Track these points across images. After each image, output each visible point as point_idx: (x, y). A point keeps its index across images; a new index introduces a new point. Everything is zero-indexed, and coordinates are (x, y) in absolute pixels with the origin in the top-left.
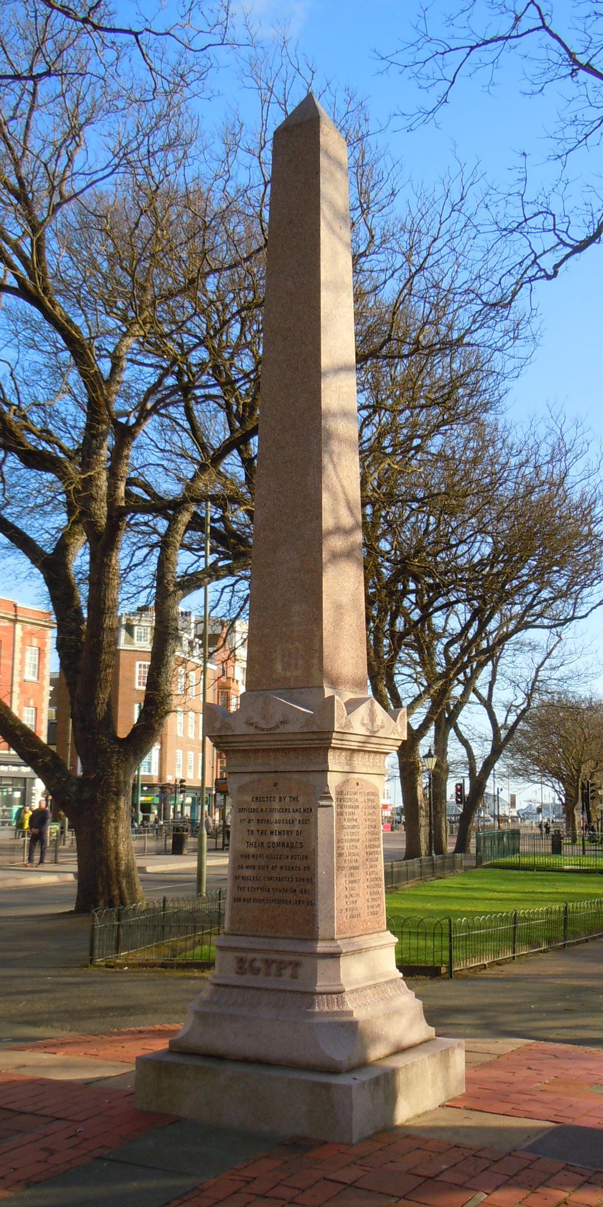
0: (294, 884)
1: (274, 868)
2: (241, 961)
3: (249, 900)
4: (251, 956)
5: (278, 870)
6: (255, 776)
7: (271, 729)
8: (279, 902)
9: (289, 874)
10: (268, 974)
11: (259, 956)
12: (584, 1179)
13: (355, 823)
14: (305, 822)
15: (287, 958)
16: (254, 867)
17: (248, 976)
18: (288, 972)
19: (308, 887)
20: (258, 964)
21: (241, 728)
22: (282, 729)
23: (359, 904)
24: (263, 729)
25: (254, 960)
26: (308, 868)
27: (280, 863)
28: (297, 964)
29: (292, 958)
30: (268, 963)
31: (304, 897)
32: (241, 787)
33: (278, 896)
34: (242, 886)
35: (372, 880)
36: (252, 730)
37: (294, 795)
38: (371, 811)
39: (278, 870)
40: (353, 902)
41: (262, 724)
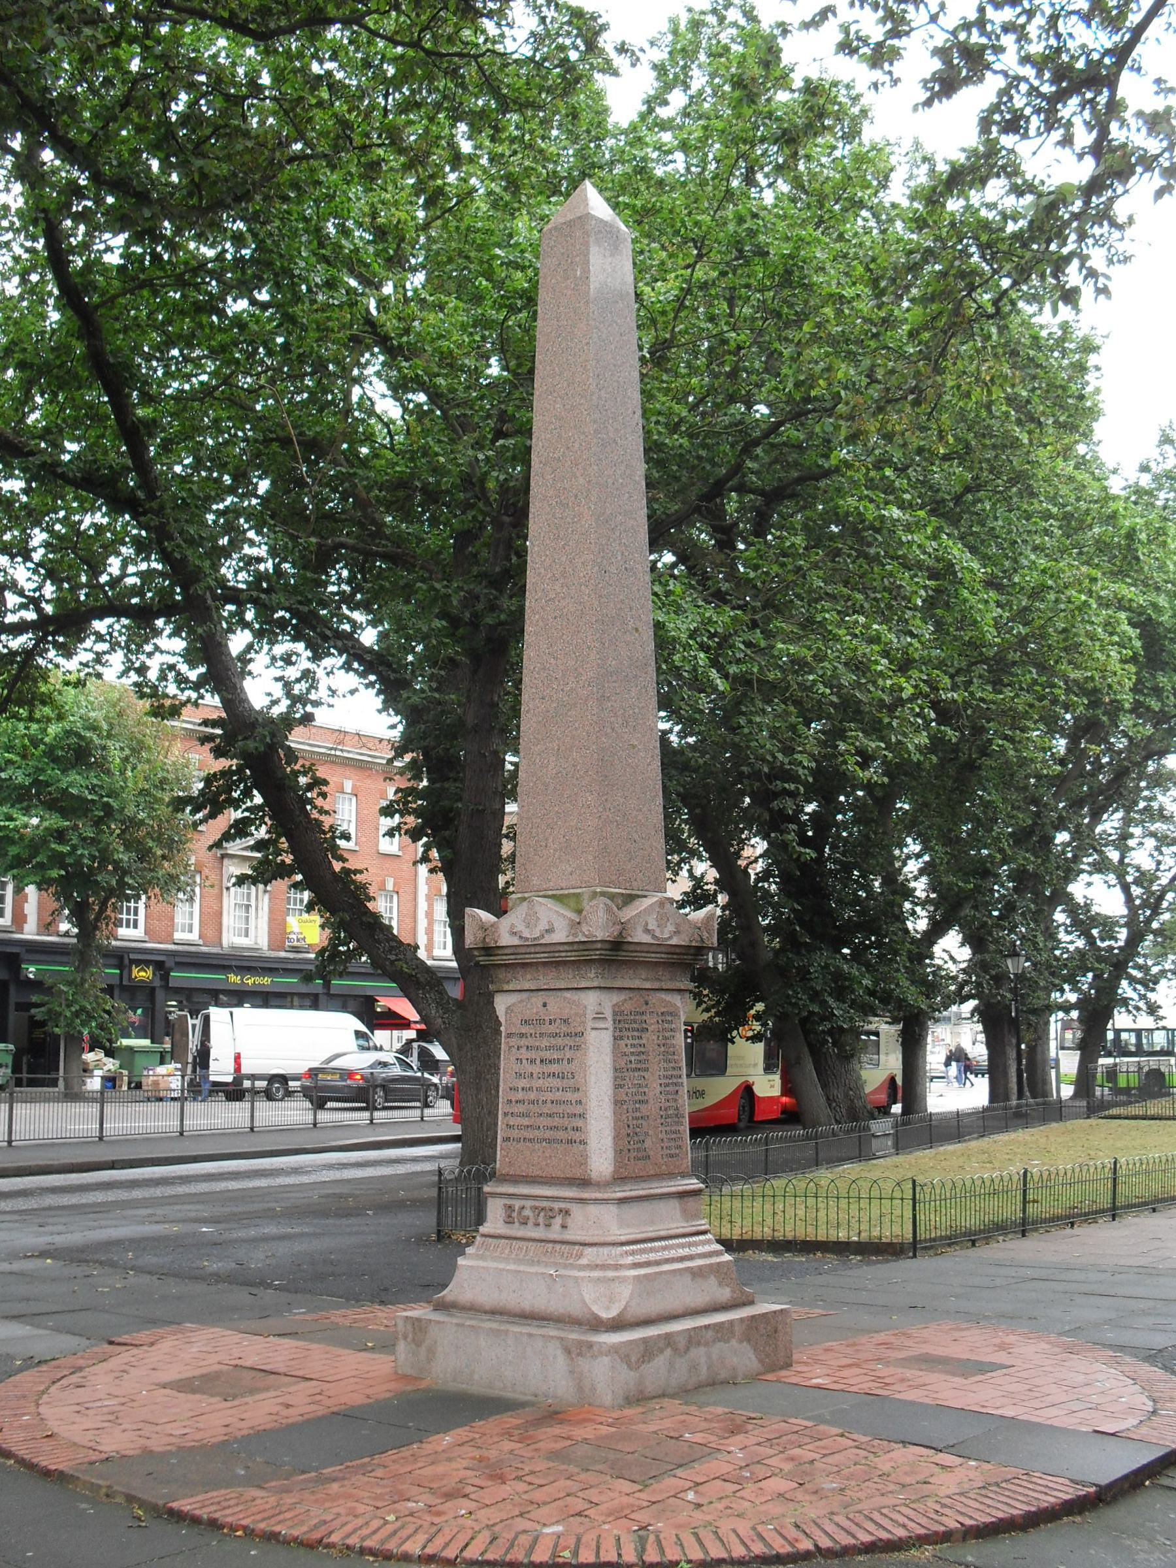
2: (510, 1208)
4: (517, 1204)
8: (549, 1141)
11: (529, 1203)
15: (557, 1206)
18: (558, 1221)
20: (527, 1212)
23: (648, 1143)
28: (567, 1212)
29: (562, 1205)
32: (508, 1008)
33: (548, 1134)
41: (526, 934)
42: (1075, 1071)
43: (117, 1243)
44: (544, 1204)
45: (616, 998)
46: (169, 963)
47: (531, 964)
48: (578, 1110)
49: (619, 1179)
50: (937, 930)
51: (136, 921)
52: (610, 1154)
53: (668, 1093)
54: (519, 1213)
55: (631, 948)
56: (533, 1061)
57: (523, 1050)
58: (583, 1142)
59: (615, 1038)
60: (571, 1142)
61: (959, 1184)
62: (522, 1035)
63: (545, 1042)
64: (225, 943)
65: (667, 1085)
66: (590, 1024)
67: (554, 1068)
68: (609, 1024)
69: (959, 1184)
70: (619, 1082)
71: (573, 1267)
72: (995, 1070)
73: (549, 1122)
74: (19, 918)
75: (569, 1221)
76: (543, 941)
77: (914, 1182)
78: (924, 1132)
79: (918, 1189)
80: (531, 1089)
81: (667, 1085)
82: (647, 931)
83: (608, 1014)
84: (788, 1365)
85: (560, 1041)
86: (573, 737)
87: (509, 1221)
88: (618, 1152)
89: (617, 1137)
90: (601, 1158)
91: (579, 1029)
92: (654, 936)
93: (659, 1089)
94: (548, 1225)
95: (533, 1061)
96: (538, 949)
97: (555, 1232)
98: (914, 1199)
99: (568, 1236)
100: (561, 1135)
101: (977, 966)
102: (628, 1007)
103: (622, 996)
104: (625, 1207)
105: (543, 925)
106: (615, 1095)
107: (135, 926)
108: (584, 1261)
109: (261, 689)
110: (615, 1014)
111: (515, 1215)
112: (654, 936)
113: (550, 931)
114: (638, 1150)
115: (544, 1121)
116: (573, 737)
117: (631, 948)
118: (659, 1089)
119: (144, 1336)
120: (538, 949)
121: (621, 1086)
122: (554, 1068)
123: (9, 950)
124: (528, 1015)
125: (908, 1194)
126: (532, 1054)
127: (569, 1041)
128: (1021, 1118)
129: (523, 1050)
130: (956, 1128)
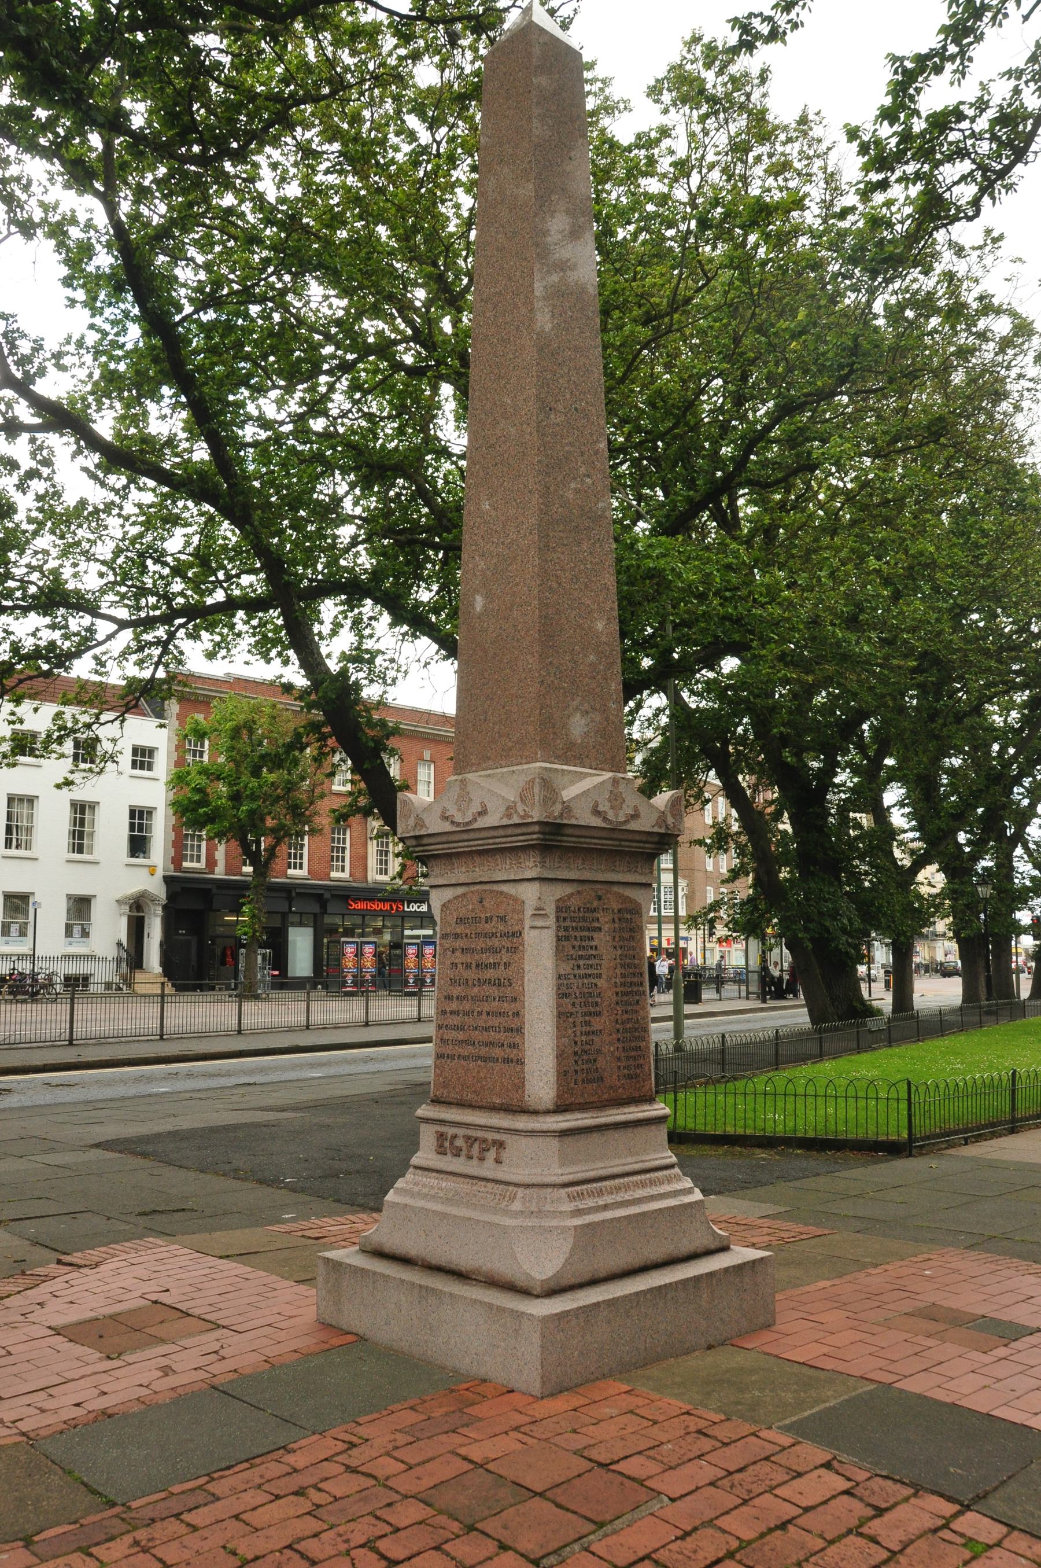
0: (502, 1036)
1: (480, 1013)
2: (441, 1136)
3: (453, 1057)
4: (451, 1131)
5: (484, 1017)
6: (460, 891)
7: (468, 824)
8: (485, 1059)
9: (496, 1021)
10: (470, 1157)
11: (461, 1132)
12: (848, 1485)
13: (593, 952)
14: (514, 950)
15: (491, 1136)
16: (457, 1013)
17: (449, 1157)
18: (492, 1154)
19: (517, 1040)
20: (459, 1142)
21: (435, 825)
22: (481, 823)
23: (601, 1063)
24: (458, 824)
25: (454, 1137)
26: (517, 1014)
27: (486, 1008)
28: (501, 1145)
29: (497, 1136)
30: (470, 1140)
31: (513, 1054)
32: (443, 905)
33: (484, 1051)
34: (446, 1037)
35: (626, 1031)
36: (448, 827)
37: (502, 914)
38: (626, 935)
39: (484, 1017)
40: (589, 1061)
41: (458, 819)
42: (298, 974)
43: (158, 1137)
44: (479, 1134)
45: (561, 891)
46: (327, 895)
47: (458, 855)
48: (515, 1023)
49: (560, 1108)
50: (920, 862)
51: (301, 864)
52: (552, 1077)
53: (626, 1003)
54: (451, 1143)
55: (569, 831)
56: (468, 966)
57: (458, 954)
58: (520, 1062)
59: (559, 939)
60: (507, 1061)
61: (951, 1085)
62: (457, 936)
63: (480, 944)
64: (369, 879)
65: (626, 994)
66: (528, 923)
67: (491, 974)
68: (551, 921)
69: (951, 1085)
70: (564, 989)
71: (506, 1212)
72: (969, 974)
73: (484, 1037)
74: (211, 863)
75: (505, 1155)
76: (475, 826)
77: (909, 1084)
78: (909, 1024)
79: (913, 1089)
80: (465, 997)
81: (626, 994)
82: (596, 812)
83: (551, 909)
84: (768, 1326)
85: (496, 942)
86: (514, 594)
87: (441, 1151)
88: (562, 1074)
89: (560, 1056)
90: (541, 1081)
91: (516, 928)
92: (605, 819)
93: (614, 998)
94: (482, 1159)
95: (468, 966)
96: (472, 835)
97: (488, 1169)
98: (909, 1100)
99: (500, 1176)
100: (497, 1052)
101: (949, 892)
102: (575, 903)
103: (569, 889)
104: (569, 1140)
105: (476, 808)
106: (558, 1005)
107: (301, 868)
108: (517, 1206)
109: (334, 649)
110: (559, 909)
111: (447, 1144)
112: (605, 819)
113: (483, 813)
114: (588, 1071)
115: (476, 1036)
116: (514, 594)
117: (569, 831)
118: (614, 998)
119: (95, 1254)
120: (472, 835)
121: (566, 995)
122: (491, 974)
123: (203, 886)
124: (463, 913)
125: (904, 1095)
126: (467, 958)
127: (506, 943)
128: (993, 1014)
129: (458, 954)
130: (939, 1025)
